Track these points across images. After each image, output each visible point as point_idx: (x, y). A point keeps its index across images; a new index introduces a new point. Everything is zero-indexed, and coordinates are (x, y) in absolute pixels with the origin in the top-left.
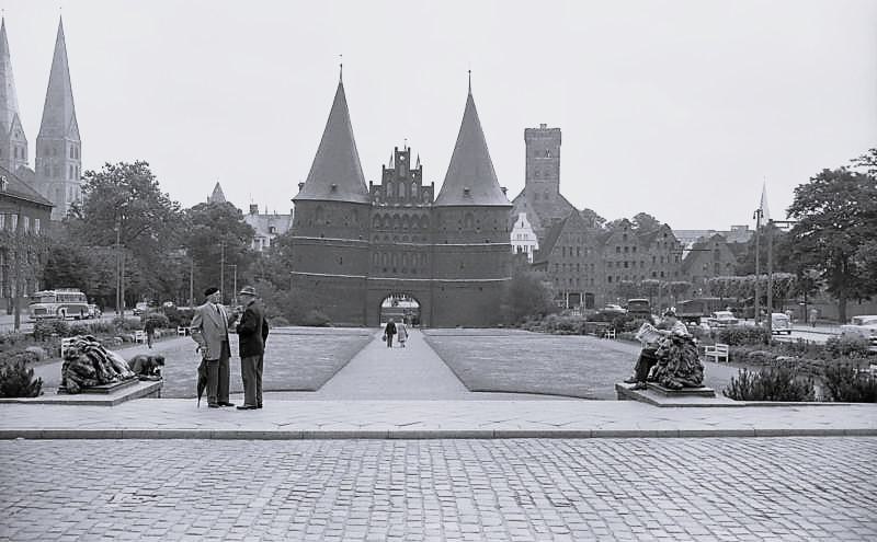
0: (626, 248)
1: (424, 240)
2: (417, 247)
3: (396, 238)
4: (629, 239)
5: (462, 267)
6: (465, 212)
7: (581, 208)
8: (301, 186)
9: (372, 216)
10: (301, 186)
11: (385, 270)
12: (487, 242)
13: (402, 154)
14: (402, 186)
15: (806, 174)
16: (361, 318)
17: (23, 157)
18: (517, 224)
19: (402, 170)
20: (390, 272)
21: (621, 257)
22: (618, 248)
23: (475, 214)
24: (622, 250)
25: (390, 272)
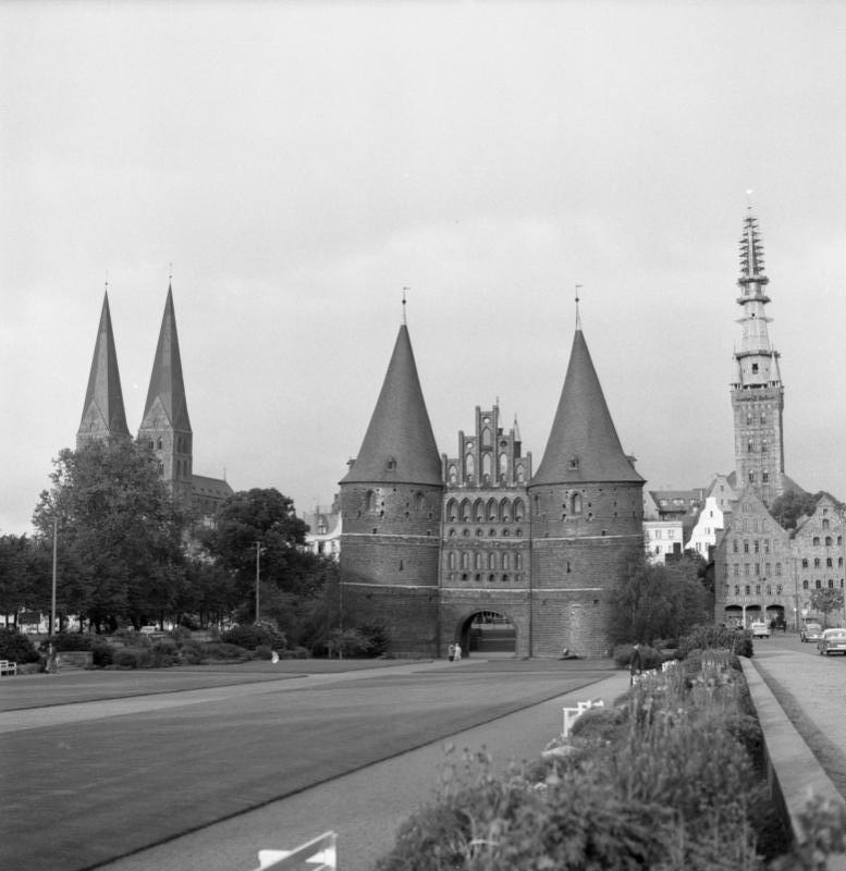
0: (828, 539)
1: (518, 532)
2: (508, 544)
3: (505, 532)
4: (832, 526)
5: (569, 571)
6: (571, 491)
7: (248, 490)
8: (351, 463)
9: (446, 501)
10: (351, 463)
11: (465, 577)
12: (604, 533)
13: (487, 415)
14: (487, 460)
15: (286, 492)
16: (433, 646)
17: (179, 462)
18: (705, 514)
19: (492, 437)
20: (471, 580)
21: (821, 552)
22: (816, 539)
23: (585, 495)
24: (823, 541)
25: (471, 580)
